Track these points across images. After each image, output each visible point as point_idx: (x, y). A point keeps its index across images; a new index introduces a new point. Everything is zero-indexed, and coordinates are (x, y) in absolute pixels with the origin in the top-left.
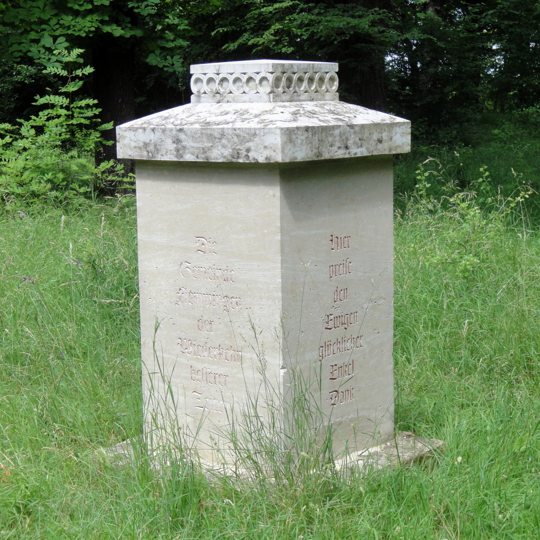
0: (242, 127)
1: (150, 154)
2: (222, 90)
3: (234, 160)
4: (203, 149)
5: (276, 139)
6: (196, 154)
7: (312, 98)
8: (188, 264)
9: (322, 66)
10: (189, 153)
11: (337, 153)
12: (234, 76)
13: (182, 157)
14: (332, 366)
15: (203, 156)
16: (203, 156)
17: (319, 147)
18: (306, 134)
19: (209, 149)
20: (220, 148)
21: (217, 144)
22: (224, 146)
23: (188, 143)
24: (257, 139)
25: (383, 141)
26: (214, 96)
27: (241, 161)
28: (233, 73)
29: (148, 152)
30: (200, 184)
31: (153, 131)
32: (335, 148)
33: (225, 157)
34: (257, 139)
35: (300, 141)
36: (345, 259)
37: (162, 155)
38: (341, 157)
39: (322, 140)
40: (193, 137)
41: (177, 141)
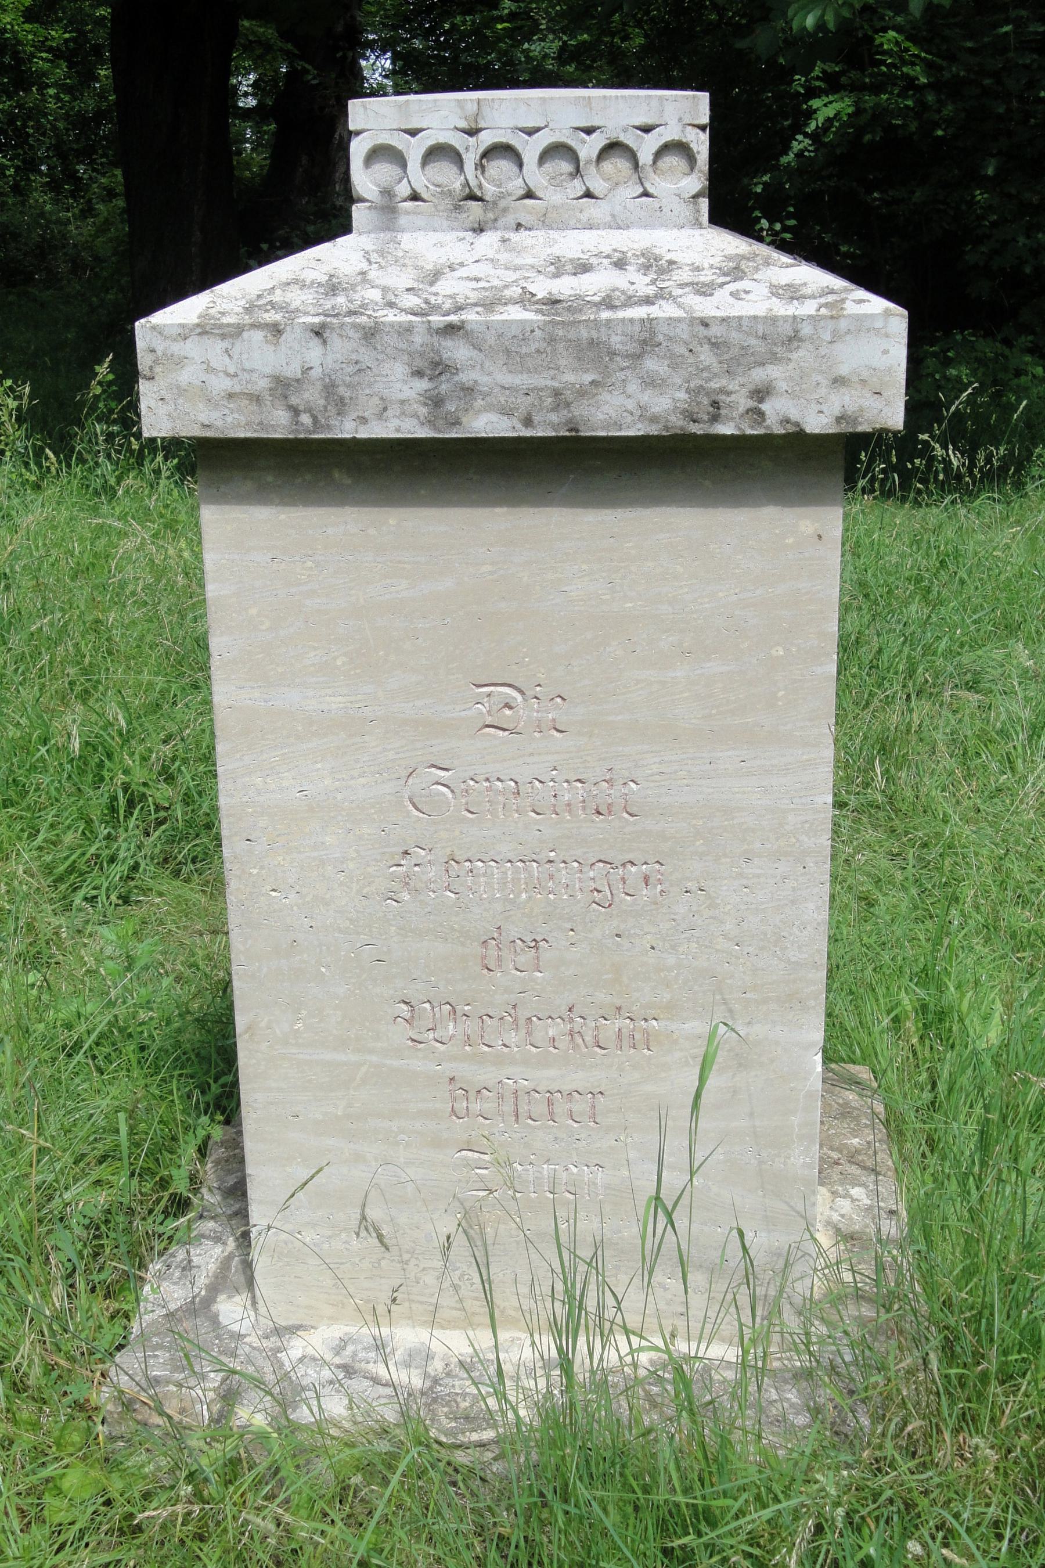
0: (734, 313)
1: (306, 419)
2: (490, 190)
3: (696, 429)
4: (557, 393)
5: (886, 352)
6: (522, 412)
8: (442, 773)
10: (488, 408)
12: (543, 140)
13: (457, 423)
15: (554, 417)
16: (554, 417)
19: (582, 393)
20: (632, 387)
21: (621, 375)
22: (651, 382)
23: (490, 375)
24: (802, 355)
26: (457, 208)
27: (726, 429)
28: (538, 130)
29: (295, 411)
30: (498, 510)
31: (317, 334)
33: (654, 419)
34: (801, 353)
37: (363, 420)
40: (508, 352)
41: (436, 368)
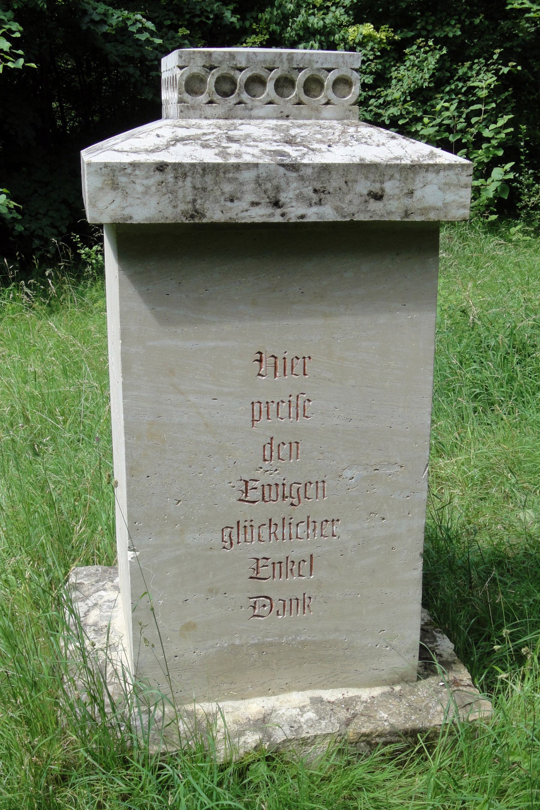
7: (286, 114)
9: (315, 58)
11: (245, 214)
14: (258, 560)
17: (194, 201)
18: (158, 176)
25: (385, 198)
32: (243, 204)
35: (140, 189)
36: (295, 393)
38: (258, 220)
39: (204, 189)
